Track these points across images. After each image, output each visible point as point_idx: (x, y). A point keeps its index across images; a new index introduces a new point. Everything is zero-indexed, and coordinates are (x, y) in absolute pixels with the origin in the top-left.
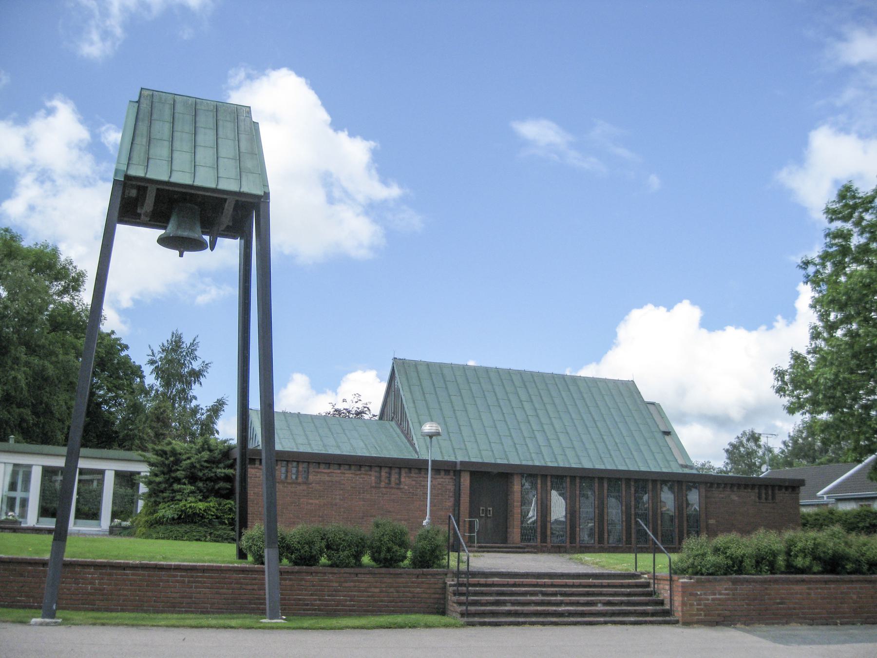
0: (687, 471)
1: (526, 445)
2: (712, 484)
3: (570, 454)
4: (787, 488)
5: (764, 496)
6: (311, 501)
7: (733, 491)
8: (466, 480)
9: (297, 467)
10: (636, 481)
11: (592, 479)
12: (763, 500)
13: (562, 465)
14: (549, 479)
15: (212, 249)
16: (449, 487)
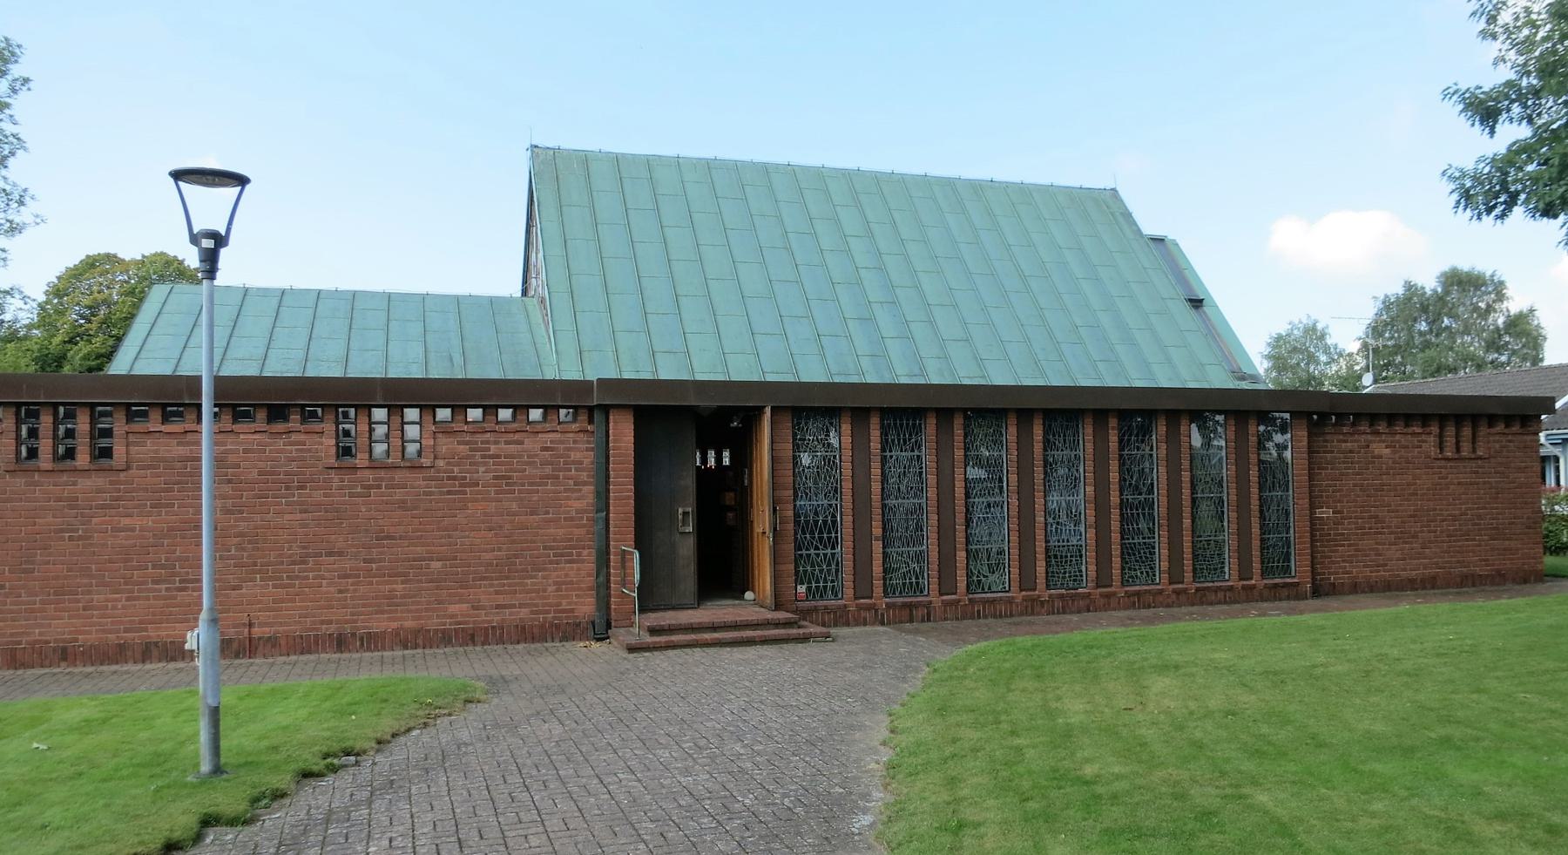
0: (1245, 385)
1: (850, 338)
2: (1324, 416)
3: (895, 349)
4: (1508, 420)
5: (45, 445)
6: (125, 521)
7: (1377, 433)
8: (623, 432)
9: (1442, 428)
10: (1124, 415)
11: (999, 414)
12: (83, 458)
13: (935, 380)
14: (875, 421)
15: (1502, 216)
16: (574, 456)
